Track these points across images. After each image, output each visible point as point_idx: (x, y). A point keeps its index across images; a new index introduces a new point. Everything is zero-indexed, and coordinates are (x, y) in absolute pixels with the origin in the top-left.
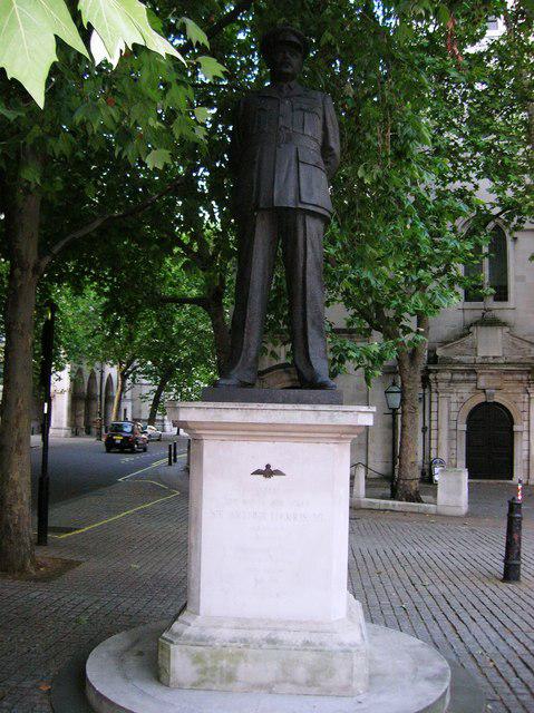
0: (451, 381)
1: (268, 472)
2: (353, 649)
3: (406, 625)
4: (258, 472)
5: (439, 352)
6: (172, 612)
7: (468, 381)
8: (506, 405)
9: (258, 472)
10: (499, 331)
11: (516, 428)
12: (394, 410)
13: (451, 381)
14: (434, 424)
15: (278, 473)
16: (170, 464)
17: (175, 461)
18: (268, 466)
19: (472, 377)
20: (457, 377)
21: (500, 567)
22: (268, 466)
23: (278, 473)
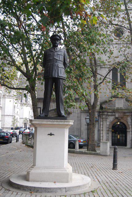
0: (107, 115)
1: (51, 134)
2: (17, 132)
3: (80, 172)
4: (49, 134)
5: (104, 106)
6: (23, 137)
7: (112, 115)
8: (125, 124)
9: (49, 134)
10: (122, 100)
11: (128, 130)
12: (88, 124)
13: (107, 115)
14: (101, 128)
15: (53, 135)
16: (17, 142)
17: (18, 141)
18: (51, 133)
19: (114, 114)
20: (109, 114)
21: (112, 167)
22: (51, 133)
23: (53, 135)
